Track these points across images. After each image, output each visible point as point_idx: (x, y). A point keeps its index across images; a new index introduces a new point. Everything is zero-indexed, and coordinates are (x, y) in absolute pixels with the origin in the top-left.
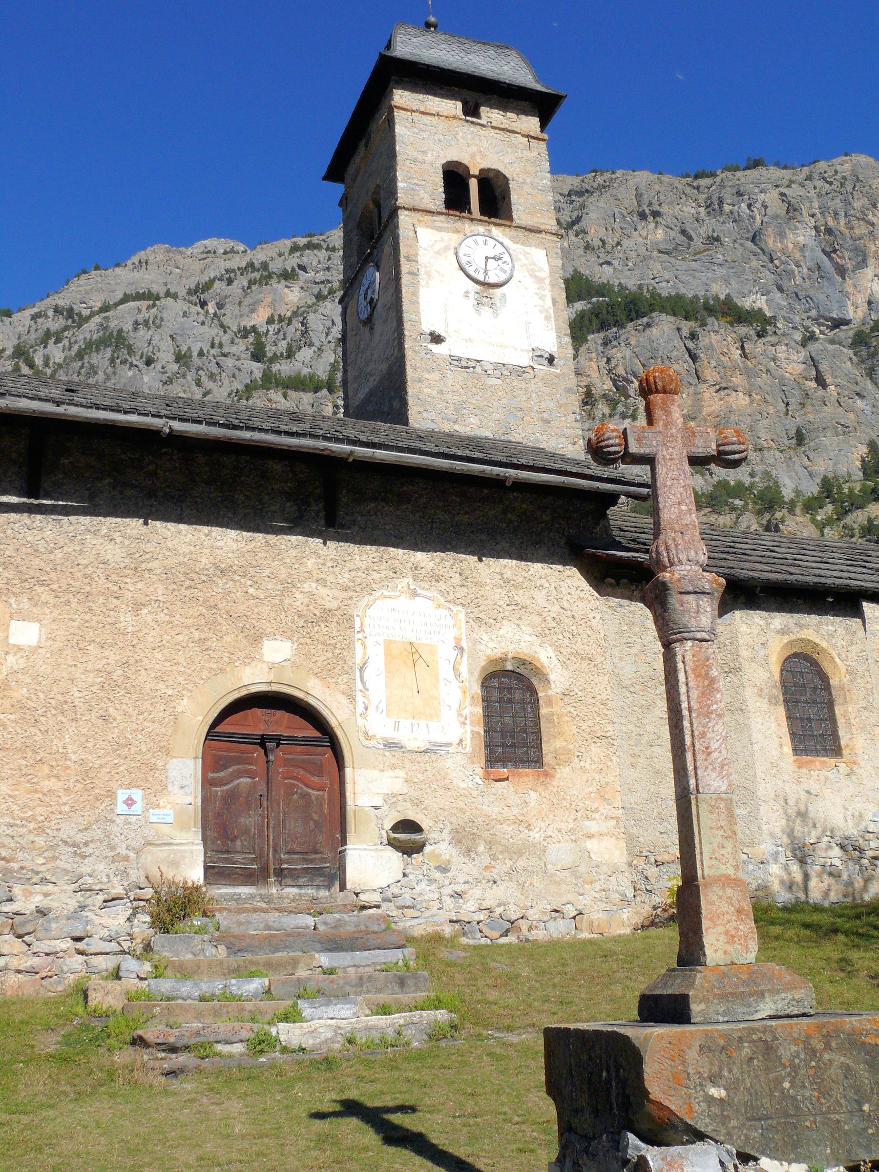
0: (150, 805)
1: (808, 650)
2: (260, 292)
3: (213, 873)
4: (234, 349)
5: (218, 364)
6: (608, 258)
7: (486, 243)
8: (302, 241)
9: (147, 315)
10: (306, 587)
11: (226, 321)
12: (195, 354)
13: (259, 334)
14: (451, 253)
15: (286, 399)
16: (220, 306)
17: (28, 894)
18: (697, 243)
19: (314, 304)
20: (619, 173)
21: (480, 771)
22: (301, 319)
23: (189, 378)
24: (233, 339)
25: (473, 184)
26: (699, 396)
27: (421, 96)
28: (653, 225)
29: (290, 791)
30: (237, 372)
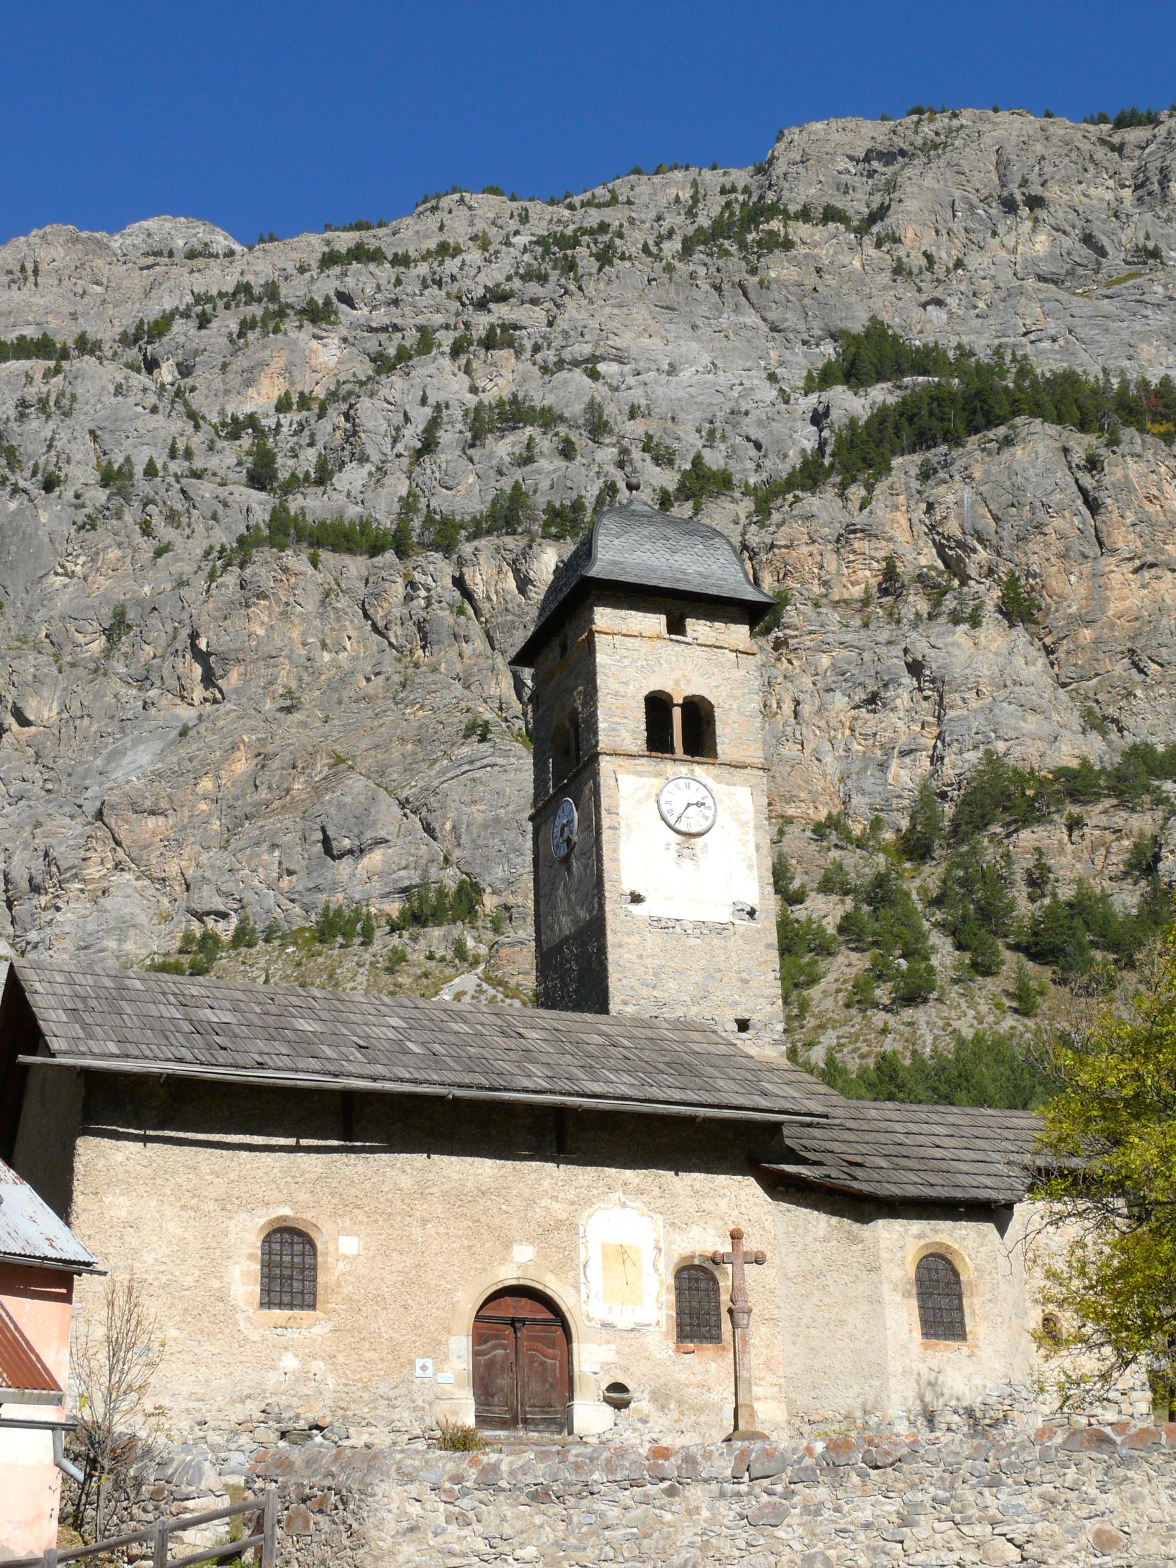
0: (438, 1370)
1: (942, 1251)
2: (264, 347)
3: (481, 1420)
4: (213, 462)
5: (183, 492)
6: (938, 293)
7: (688, 786)
8: (345, 240)
9: (45, 389)
10: (543, 1203)
11: (197, 401)
12: (139, 470)
13: (263, 432)
14: (654, 799)
15: (315, 567)
16: (185, 370)
17: (359, 1433)
18: (1115, 261)
19: (370, 378)
20: (967, 117)
21: (672, 1346)
22: (344, 407)
23: (128, 518)
24: (212, 441)
25: (677, 713)
26: (1101, 580)
27: (623, 613)
28: (1029, 224)
29: (532, 1360)
30: (220, 508)
